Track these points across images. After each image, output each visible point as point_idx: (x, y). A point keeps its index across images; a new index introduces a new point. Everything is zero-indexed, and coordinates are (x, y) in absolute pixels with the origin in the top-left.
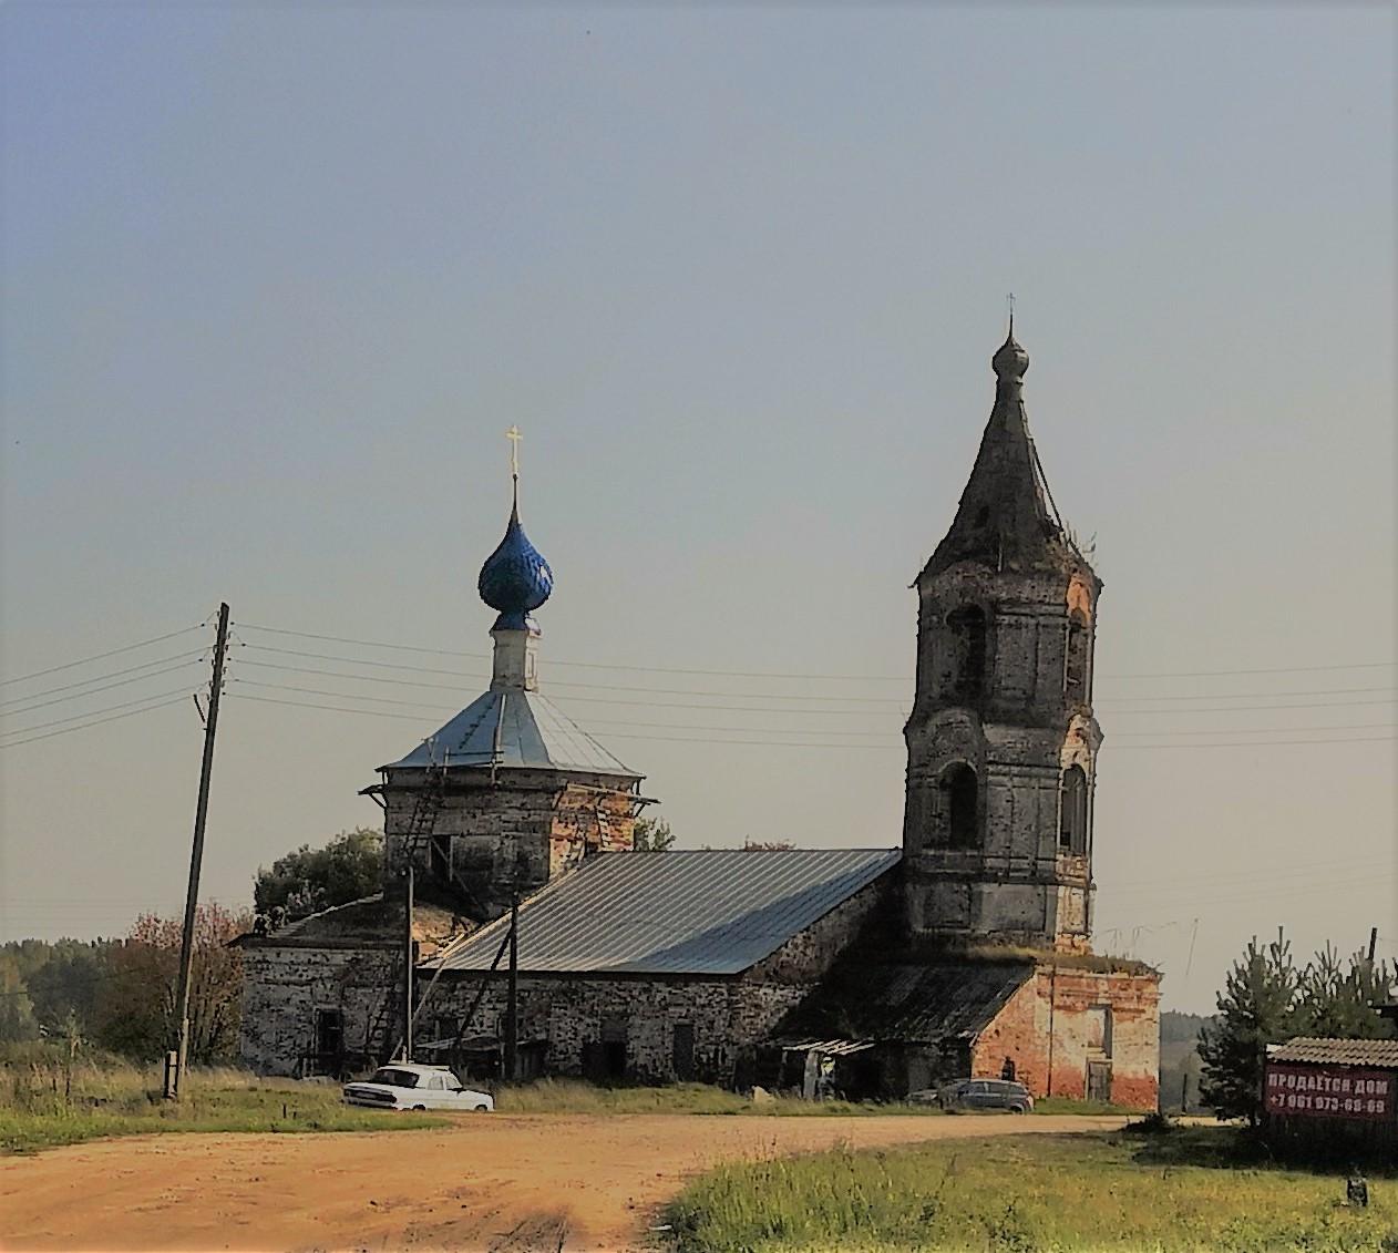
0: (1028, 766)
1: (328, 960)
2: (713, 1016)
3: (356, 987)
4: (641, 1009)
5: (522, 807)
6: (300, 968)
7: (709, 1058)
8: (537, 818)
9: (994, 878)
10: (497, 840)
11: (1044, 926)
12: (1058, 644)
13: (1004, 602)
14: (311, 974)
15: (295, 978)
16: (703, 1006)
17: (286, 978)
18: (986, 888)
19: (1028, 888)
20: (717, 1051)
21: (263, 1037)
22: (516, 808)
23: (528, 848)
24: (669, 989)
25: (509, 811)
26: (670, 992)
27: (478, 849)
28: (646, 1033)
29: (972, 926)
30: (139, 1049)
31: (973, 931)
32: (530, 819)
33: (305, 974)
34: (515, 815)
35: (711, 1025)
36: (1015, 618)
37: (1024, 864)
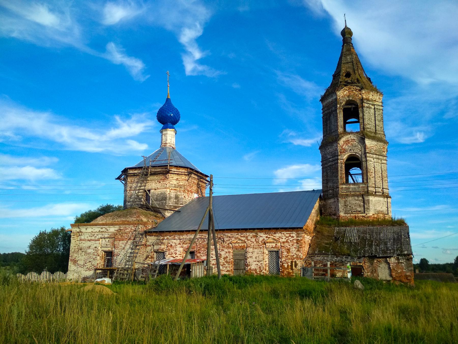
0: (379, 155)
1: (107, 230)
2: (289, 246)
3: (120, 241)
4: (253, 244)
5: (177, 179)
6: (95, 234)
7: (288, 265)
8: (182, 184)
9: (372, 195)
10: (168, 190)
11: (388, 213)
12: (381, 115)
13: (365, 99)
14: (100, 236)
15: (93, 238)
16: (284, 242)
17: (90, 238)
18: (371, 198)
19: (382, 199)
20: (292, 262)
21: (78, 262)
22: (175, 180)
23: (179, 193)
24: (267, 235)
25: (173, 181)
26: (267, 237)
27: (162, 193)
28: (255, 255)
29: (366, 212)
30: (392, 222)
31: (367, 214)
32: (179, 184)
33: (97, 236)
34: (175, 182)
35: (288, 250)
36: (368, 105)
37: (380, 190)
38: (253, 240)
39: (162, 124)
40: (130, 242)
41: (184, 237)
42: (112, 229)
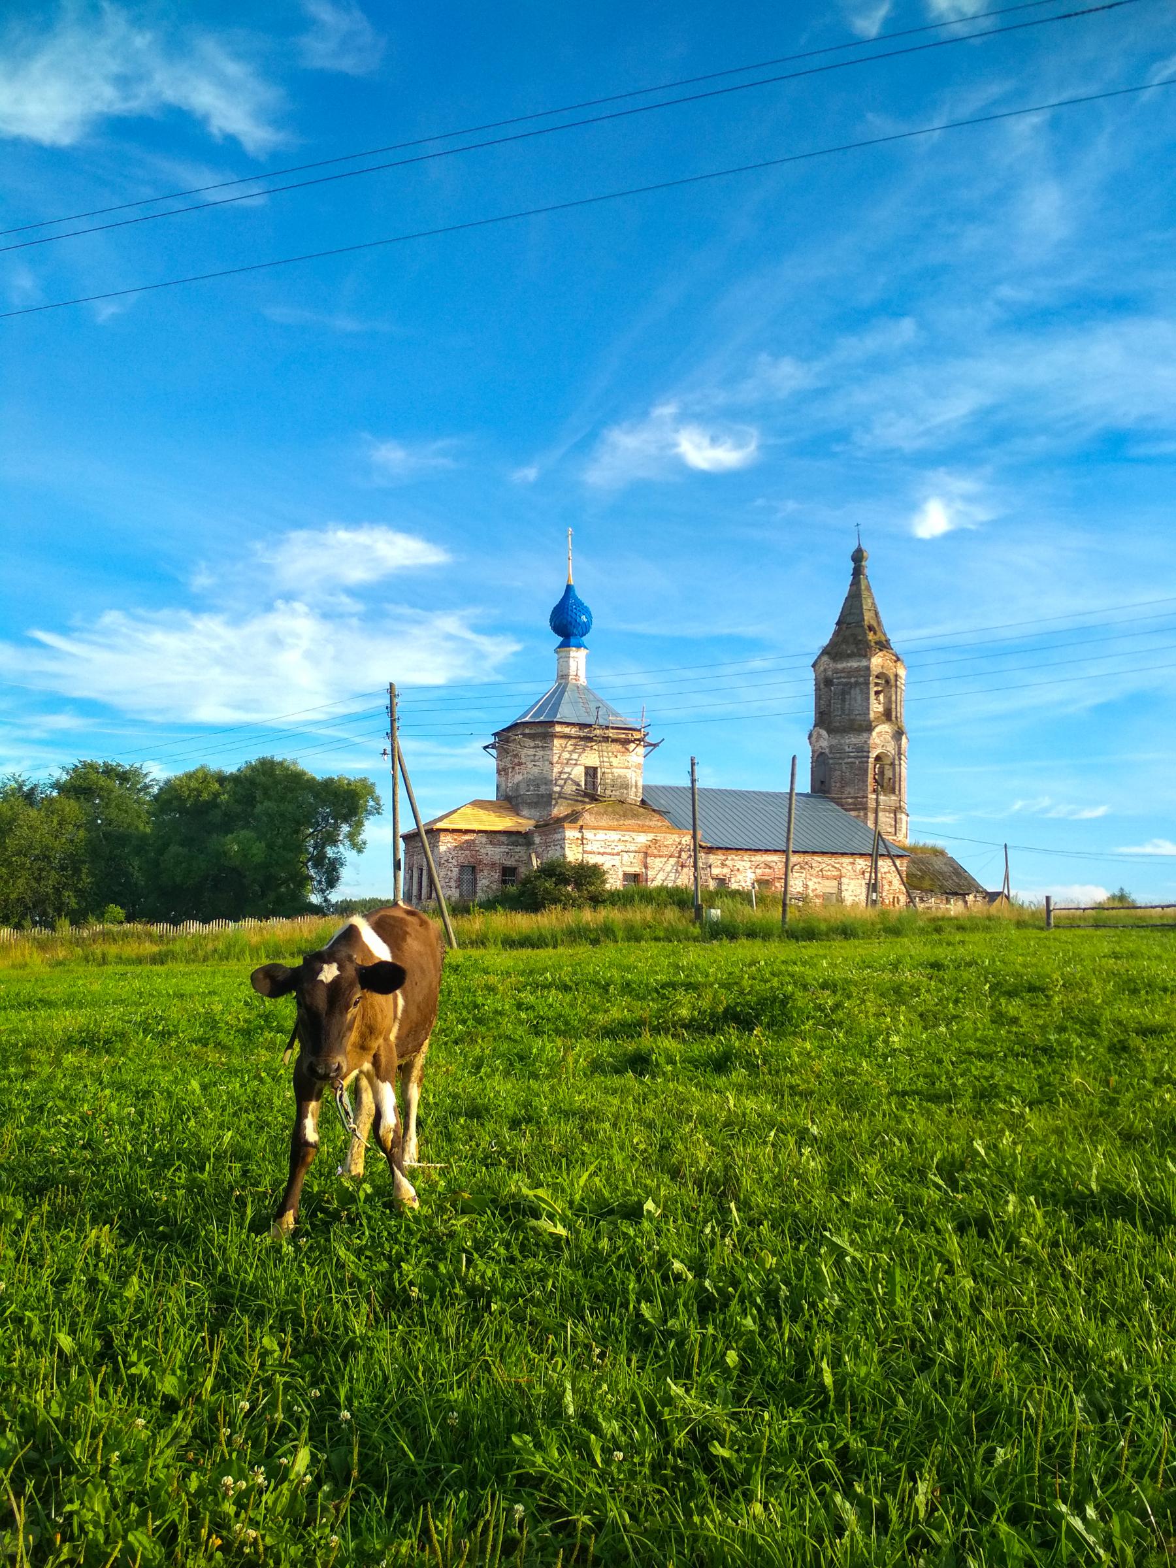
15: (608, 850)
17: (602, 850)
28: (851, 888)
38: (850, 867)
39: (560, 635)
40: (673, 861)
41: (759, 858)
42: (643, 839)
